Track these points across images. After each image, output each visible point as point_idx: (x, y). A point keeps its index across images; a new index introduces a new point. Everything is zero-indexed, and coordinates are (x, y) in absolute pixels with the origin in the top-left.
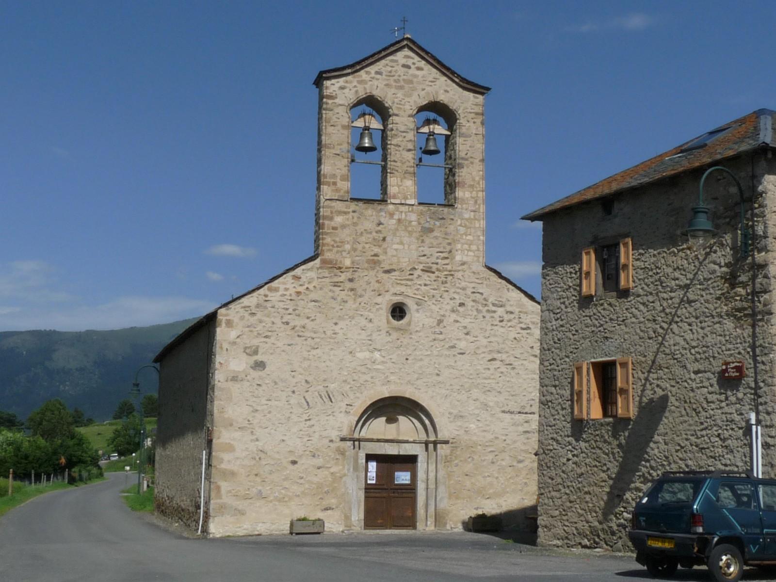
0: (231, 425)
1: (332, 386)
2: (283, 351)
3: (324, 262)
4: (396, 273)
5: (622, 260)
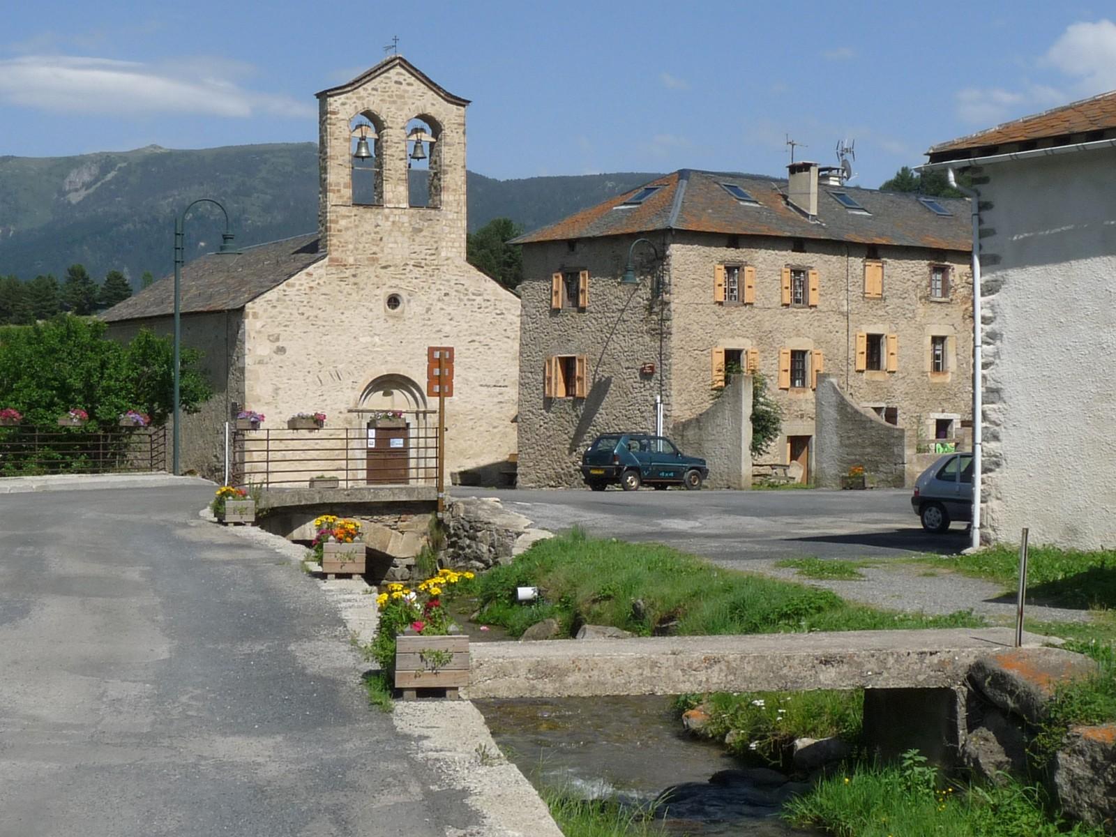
0: (259, 401)
1: (340, 366)
2: (300, 338)
3: (331, 260)
4: (392, 268)
5: (581, 286)
